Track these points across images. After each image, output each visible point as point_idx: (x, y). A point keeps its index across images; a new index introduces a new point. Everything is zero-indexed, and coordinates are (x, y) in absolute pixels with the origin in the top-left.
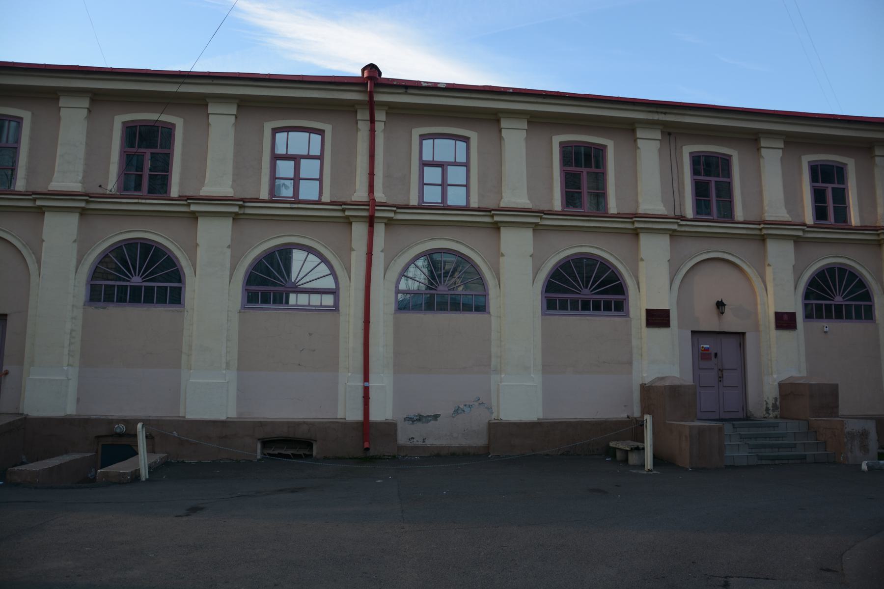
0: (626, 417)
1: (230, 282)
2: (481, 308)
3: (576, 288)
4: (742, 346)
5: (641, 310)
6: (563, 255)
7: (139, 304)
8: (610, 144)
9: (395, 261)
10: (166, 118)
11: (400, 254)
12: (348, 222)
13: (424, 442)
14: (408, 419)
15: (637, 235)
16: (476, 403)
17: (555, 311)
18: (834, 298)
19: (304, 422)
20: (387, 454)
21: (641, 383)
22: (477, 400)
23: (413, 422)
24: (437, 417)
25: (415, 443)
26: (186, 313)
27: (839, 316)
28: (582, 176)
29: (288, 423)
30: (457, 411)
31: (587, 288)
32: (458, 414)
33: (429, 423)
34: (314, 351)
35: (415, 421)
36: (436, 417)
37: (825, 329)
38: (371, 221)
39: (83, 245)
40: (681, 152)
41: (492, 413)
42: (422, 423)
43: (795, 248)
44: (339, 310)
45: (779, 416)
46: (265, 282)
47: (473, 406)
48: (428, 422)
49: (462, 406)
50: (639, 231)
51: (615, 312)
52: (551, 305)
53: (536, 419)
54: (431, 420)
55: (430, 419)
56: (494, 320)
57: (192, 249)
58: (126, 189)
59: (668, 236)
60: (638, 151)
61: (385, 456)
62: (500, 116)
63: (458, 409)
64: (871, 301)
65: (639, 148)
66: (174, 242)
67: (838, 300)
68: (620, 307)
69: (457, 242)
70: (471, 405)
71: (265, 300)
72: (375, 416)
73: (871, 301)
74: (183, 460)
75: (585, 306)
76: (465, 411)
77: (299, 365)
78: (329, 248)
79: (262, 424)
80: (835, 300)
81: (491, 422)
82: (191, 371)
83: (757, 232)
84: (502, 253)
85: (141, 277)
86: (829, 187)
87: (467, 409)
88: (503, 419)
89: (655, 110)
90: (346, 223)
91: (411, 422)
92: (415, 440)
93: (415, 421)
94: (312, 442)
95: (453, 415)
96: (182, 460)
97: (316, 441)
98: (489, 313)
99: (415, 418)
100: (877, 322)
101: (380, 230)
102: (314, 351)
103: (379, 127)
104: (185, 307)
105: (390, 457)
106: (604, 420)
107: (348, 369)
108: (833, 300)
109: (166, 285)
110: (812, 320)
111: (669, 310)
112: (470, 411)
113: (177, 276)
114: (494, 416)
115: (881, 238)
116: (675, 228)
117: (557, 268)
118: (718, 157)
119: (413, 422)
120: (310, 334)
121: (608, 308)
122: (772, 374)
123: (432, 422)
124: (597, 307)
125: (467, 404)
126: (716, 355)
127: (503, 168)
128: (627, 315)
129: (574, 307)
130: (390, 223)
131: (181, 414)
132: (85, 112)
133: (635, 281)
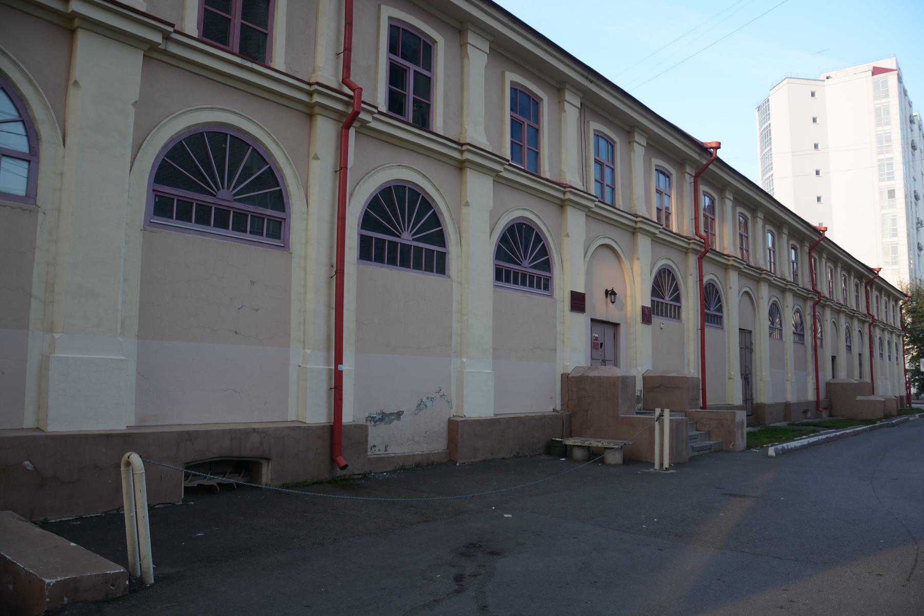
0: (552, 410)
1: (130, 170)
2: (442, 269)
3: (401, 228)
4: (616, 336)
5: (564, 291)
7: (420, 271)
9: (360, 186)
11: (164, 121)
12: (309, 113)
13: (386, 450)
14: (370, 419)
15: (311, 116)
16: (438, 395)
17: (276, 240)
18: (218, 190)
19: (254, 430)
20: (356, 472)
21: (562, 373)
22: (438, 391)
23: (375, 422)
24: (400, 415)
25: (376, 452)
26: (41, 216)
28: (523, 127)
29: (231, 431)
30: (421, 406)
31: (526, 259)
32: (421, 410)
33: (392, 424)
34: (257, 310)
35: (377, 421)
36: (399, 415)
37: (662, 326)
38: (701, 257)
40: (589, 127)
41: (451, 408)
42: (385, 424)
43: (143, 75)
44: (289, 248)
45: (642, 409)
47: (435, 398)
48: (390, 422)
49: (424, 400)
50: (77, 23)
51: (521, 286)
53: (493, 415)
54: (393, 420)
55: (393, 417)
56: (455, 286)
59: (139, 56)
60: (563, 114)
61: (354, 475)
62: (469, 27)
63: (420, 404)
64: (284, 211)
65: (565, 111)
66: (19, 63)
67: (406, 238)
69: (424, 176)
70: (433, 398)
71: (184, 215)
72: (348, 418)
73: (284, 211)
74: (46, 519)
76: (428, 405)
77: (236, 332)
78: (282, 146)
79: (190, 436)
80: (402, 237)
81: (451, 419)
82: (57, 336)
83: (633, 224)
84: (467, 201)
85: (223, 188)
87: (429, 404)
88: (467, 415)
89: (747, 185)
90: (306, 113)
91: (373, 423)
92: (377, 449)
93: (377, 421)
94: (261, 461)
95: (416, 412)
96: (42, 519)
97: (268, 459)
98: (449, 277)
99: (378, 417)
100: (683, 322)
102: (257, 310)
104: (38, 203)
105: (360, 476)
106: (541, 414)
107: (304, 342)
108: (400, 237)
109: (384, 238)
110: (370, 262)
111: (585, 294)
112: (432, 406)
114: (454, 412)
115: (690, 247)
116: (657, 233)
117: (181, 142)
118: (399, 28)
119: (375, 422)
120: (252, 283)
122: (636, 367)
123: (395, 422)
125: (430, 396)
126: (602, 344)
127: (465, 94)
128: (285, 247)
129: (203, 219)
131: (29, 422)
133: (58, 129)
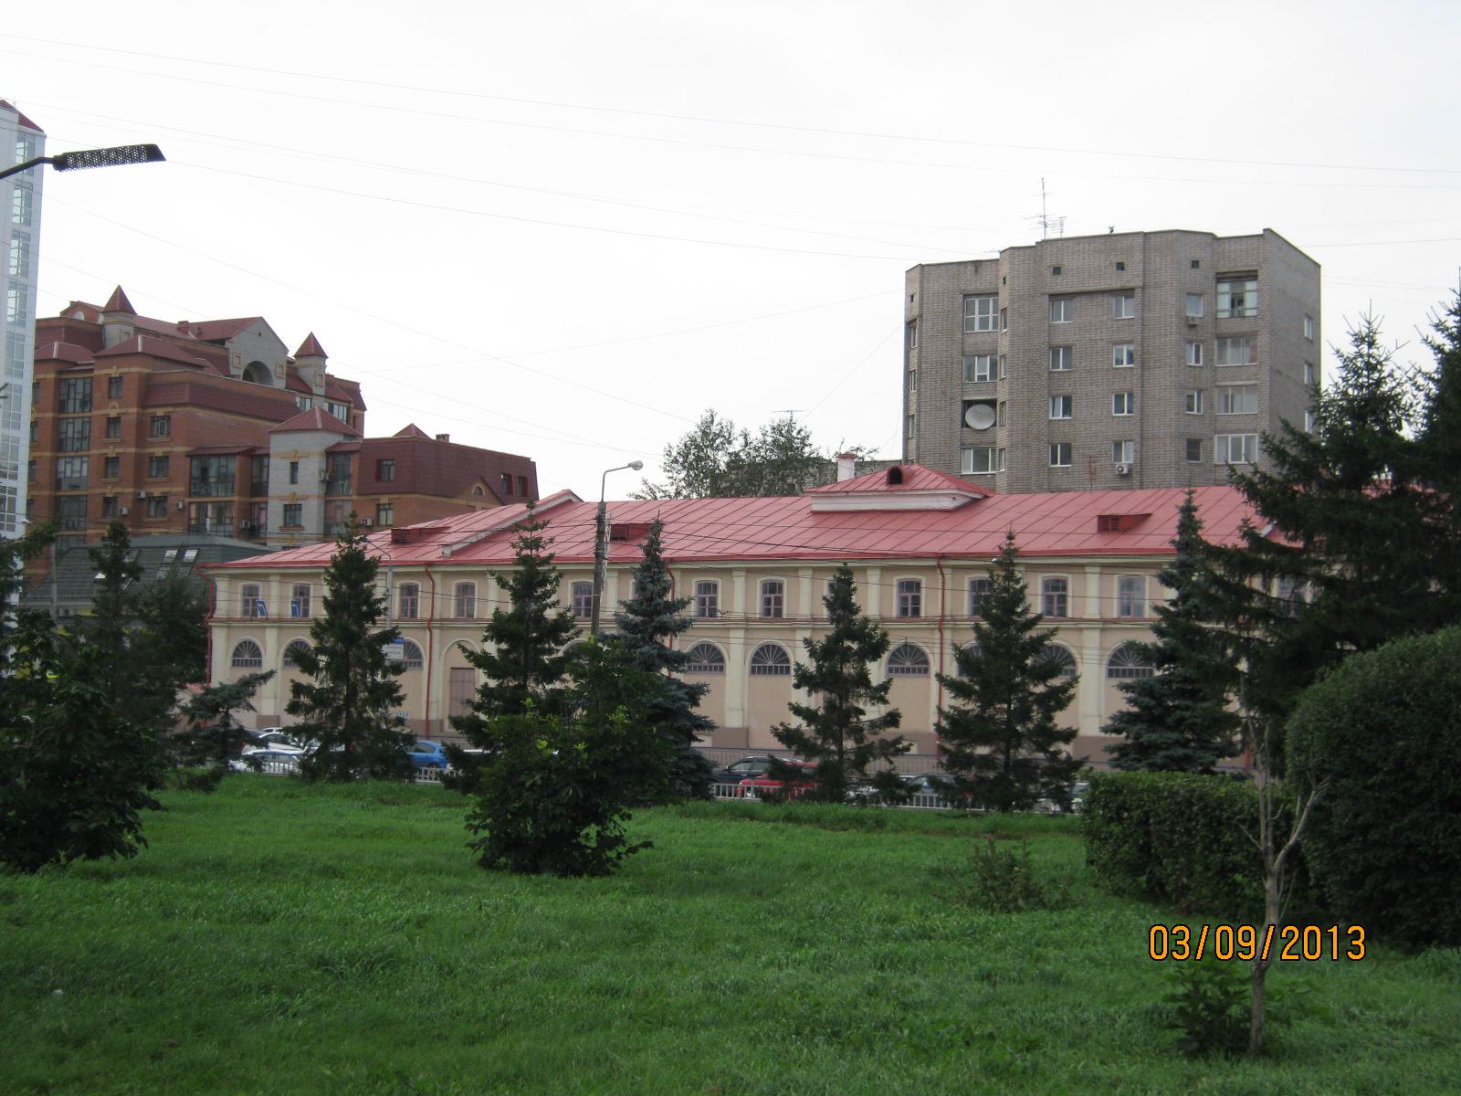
6: (417, 642)
8: (785, 581)
10: (415, 582)
27: (770, 672)
39: (279, 641)
46: (896, 663)
52: (753, 671)
57: (264, 643)
58: (703, 615)
68: (926, 671)
75: (908, 670)
86: (772, 596)
101: (436, 632)
103: (948, 577)
113: (721, 659)
121: (920, 671)
124: (914, 671)
128: (724, 675)
130: (441, 628)
132: (616, 579)
